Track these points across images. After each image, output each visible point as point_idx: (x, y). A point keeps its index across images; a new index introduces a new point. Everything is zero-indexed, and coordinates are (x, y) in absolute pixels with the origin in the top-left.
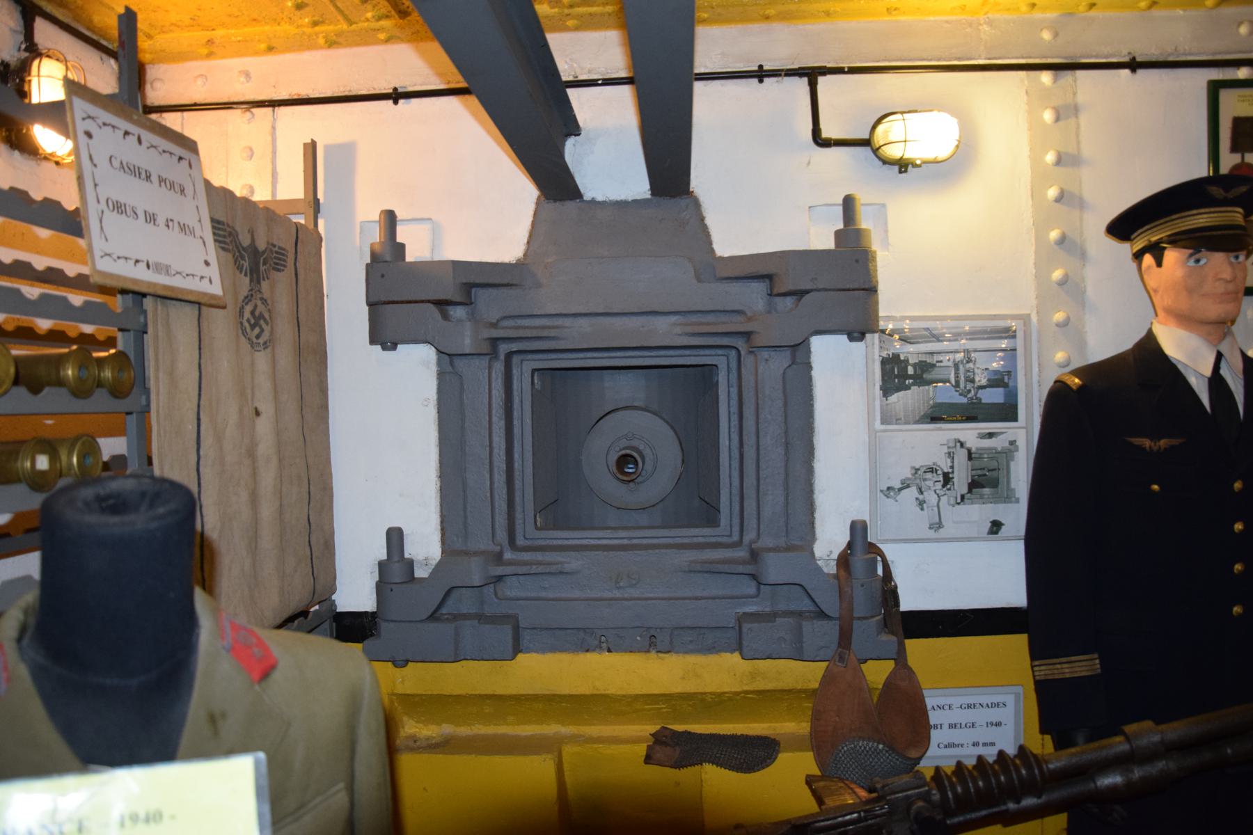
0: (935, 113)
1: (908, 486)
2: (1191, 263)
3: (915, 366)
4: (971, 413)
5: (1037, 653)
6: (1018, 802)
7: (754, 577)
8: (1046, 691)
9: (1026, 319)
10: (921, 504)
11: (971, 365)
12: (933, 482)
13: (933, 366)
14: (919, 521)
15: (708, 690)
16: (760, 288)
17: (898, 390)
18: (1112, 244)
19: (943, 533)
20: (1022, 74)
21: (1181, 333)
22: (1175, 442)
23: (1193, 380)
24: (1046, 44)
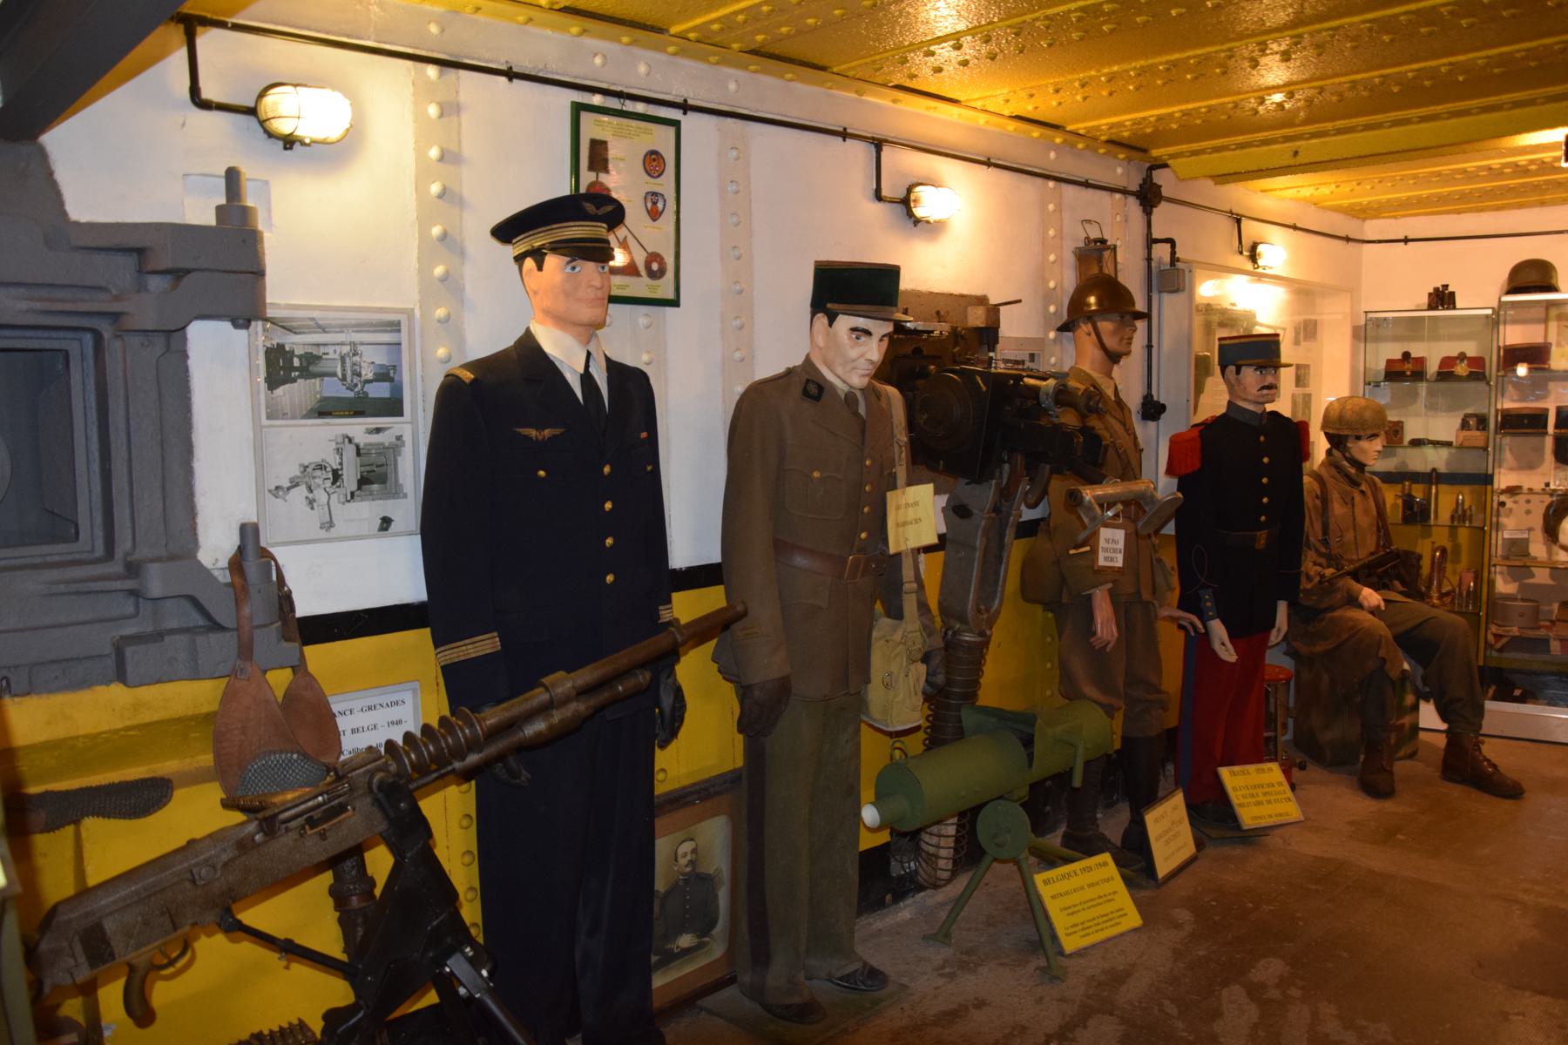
0: (327, 92)
1: (297, 485)
2: (568, 269)
3: (300, 357)
4: (358, 407)
5: (438, 642)
6: (463, 759)
7: (134, 593)
8: (451, 673)
9: (409, 313)
10: (311, 502)
11: (357, 358)
12: (322, 480)
13: (319, 358)
14: (309, 521)
15: (82, 732)
16: (130, 262)
17: (284, 382)
18: (495, 244)
19: (334, 532)
20: (409, 63)
21: (558, 333)
22: (557, 431)
23: (569, 376)
24: (432, 36)
